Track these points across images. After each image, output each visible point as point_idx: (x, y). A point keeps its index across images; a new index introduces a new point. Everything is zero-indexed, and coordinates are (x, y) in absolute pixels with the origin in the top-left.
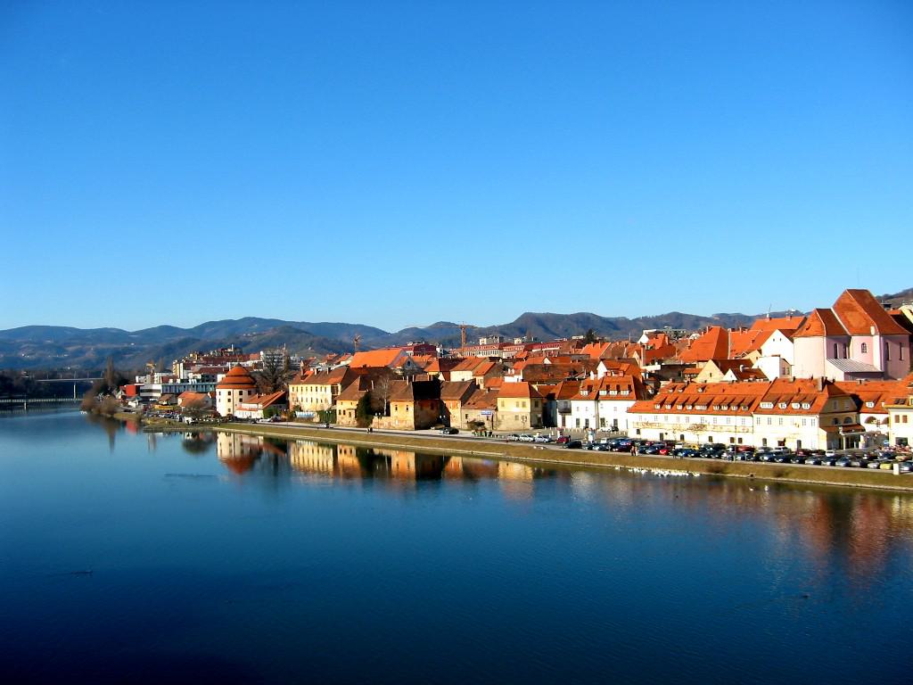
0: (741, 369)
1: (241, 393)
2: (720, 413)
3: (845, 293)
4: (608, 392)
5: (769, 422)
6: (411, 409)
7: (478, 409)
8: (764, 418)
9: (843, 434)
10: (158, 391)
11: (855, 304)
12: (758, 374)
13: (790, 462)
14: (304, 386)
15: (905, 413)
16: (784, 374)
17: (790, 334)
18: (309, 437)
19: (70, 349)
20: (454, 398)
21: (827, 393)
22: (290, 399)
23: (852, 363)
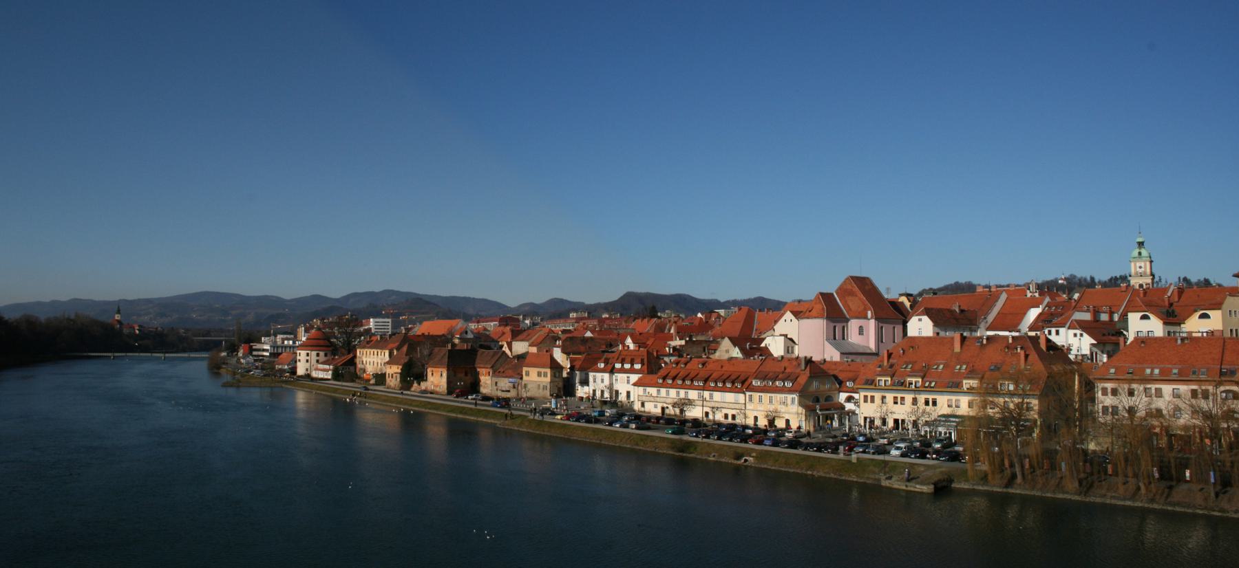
0: (748, 347)
1: (318, 355)
2: (716, 389)
3: (847, 279)
4: (623, 365)
5: (760, 399)
6: (445, 375)
7: (506, 377)
8: (756, 395)
9: (819, 413)
10: (267, 350)
11: (856, 289)
12: (766, 352)
13: (746, 442)
14: (368, 351)
15: (934, 397)
16: (788, 352)
17: (797, 314)
18: (375, 401)
19: (234, 312)
20: (486, 366)
21: (808, 372)
22: (358, 360)
23: (849, 344)
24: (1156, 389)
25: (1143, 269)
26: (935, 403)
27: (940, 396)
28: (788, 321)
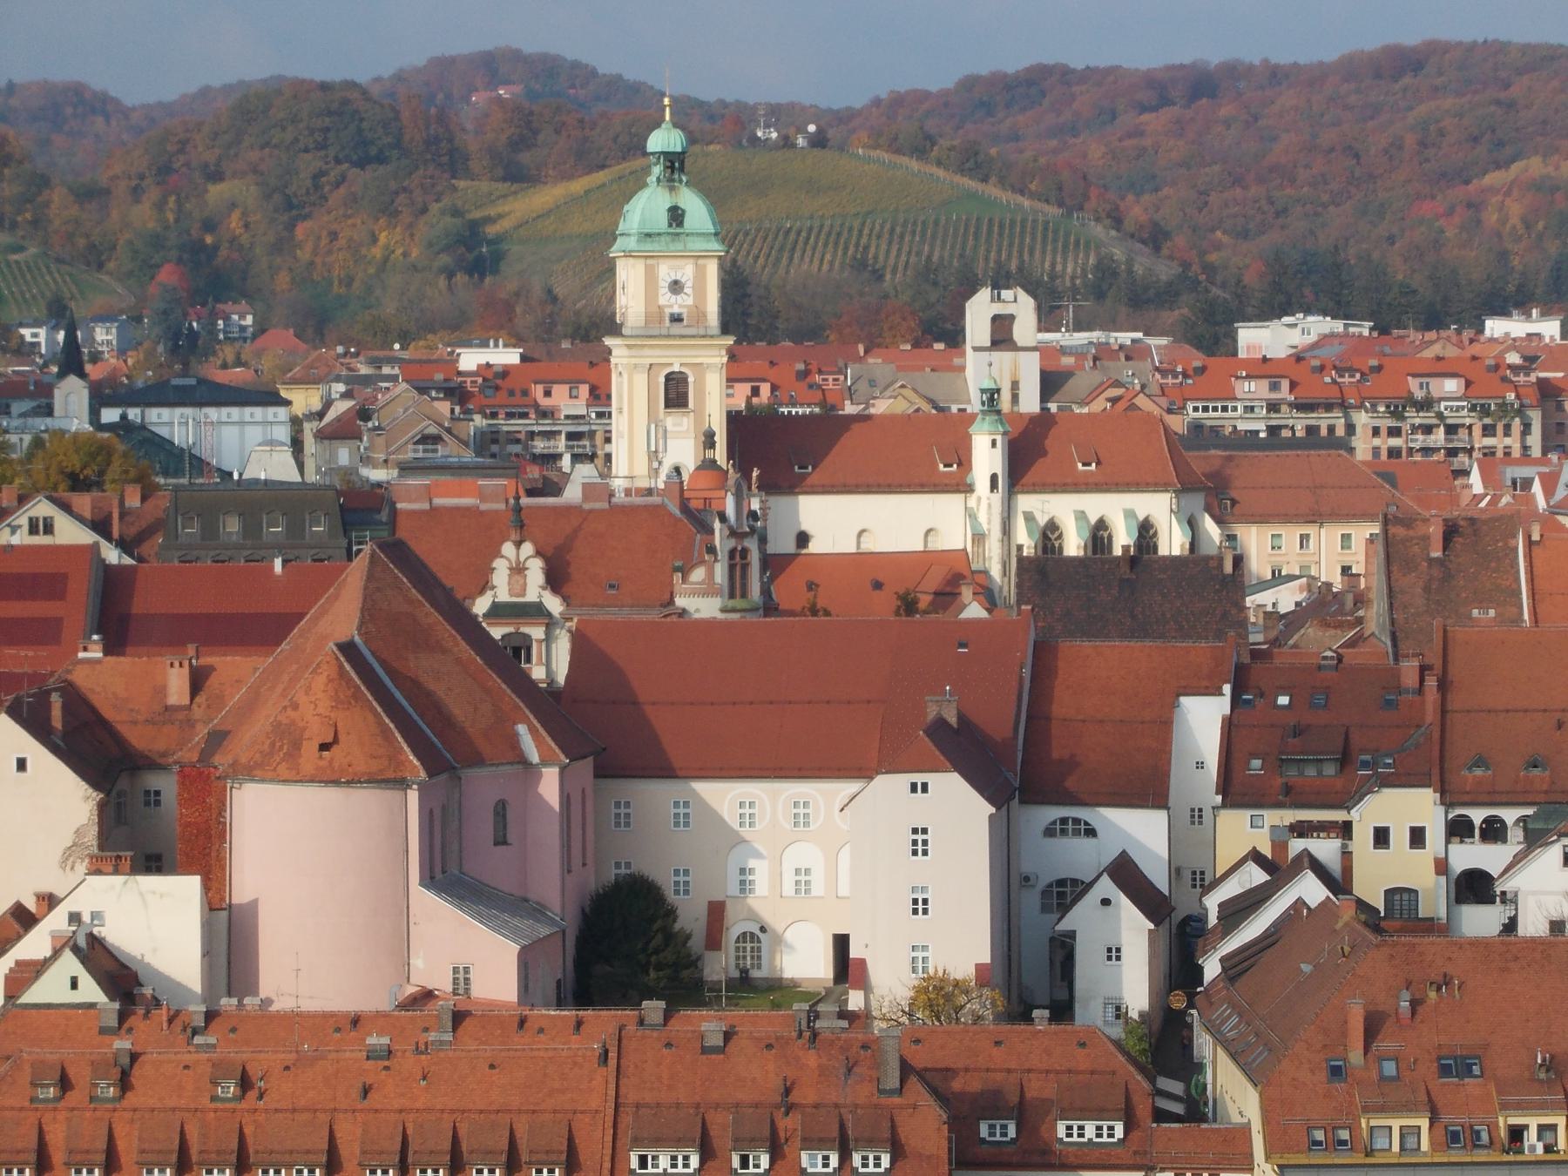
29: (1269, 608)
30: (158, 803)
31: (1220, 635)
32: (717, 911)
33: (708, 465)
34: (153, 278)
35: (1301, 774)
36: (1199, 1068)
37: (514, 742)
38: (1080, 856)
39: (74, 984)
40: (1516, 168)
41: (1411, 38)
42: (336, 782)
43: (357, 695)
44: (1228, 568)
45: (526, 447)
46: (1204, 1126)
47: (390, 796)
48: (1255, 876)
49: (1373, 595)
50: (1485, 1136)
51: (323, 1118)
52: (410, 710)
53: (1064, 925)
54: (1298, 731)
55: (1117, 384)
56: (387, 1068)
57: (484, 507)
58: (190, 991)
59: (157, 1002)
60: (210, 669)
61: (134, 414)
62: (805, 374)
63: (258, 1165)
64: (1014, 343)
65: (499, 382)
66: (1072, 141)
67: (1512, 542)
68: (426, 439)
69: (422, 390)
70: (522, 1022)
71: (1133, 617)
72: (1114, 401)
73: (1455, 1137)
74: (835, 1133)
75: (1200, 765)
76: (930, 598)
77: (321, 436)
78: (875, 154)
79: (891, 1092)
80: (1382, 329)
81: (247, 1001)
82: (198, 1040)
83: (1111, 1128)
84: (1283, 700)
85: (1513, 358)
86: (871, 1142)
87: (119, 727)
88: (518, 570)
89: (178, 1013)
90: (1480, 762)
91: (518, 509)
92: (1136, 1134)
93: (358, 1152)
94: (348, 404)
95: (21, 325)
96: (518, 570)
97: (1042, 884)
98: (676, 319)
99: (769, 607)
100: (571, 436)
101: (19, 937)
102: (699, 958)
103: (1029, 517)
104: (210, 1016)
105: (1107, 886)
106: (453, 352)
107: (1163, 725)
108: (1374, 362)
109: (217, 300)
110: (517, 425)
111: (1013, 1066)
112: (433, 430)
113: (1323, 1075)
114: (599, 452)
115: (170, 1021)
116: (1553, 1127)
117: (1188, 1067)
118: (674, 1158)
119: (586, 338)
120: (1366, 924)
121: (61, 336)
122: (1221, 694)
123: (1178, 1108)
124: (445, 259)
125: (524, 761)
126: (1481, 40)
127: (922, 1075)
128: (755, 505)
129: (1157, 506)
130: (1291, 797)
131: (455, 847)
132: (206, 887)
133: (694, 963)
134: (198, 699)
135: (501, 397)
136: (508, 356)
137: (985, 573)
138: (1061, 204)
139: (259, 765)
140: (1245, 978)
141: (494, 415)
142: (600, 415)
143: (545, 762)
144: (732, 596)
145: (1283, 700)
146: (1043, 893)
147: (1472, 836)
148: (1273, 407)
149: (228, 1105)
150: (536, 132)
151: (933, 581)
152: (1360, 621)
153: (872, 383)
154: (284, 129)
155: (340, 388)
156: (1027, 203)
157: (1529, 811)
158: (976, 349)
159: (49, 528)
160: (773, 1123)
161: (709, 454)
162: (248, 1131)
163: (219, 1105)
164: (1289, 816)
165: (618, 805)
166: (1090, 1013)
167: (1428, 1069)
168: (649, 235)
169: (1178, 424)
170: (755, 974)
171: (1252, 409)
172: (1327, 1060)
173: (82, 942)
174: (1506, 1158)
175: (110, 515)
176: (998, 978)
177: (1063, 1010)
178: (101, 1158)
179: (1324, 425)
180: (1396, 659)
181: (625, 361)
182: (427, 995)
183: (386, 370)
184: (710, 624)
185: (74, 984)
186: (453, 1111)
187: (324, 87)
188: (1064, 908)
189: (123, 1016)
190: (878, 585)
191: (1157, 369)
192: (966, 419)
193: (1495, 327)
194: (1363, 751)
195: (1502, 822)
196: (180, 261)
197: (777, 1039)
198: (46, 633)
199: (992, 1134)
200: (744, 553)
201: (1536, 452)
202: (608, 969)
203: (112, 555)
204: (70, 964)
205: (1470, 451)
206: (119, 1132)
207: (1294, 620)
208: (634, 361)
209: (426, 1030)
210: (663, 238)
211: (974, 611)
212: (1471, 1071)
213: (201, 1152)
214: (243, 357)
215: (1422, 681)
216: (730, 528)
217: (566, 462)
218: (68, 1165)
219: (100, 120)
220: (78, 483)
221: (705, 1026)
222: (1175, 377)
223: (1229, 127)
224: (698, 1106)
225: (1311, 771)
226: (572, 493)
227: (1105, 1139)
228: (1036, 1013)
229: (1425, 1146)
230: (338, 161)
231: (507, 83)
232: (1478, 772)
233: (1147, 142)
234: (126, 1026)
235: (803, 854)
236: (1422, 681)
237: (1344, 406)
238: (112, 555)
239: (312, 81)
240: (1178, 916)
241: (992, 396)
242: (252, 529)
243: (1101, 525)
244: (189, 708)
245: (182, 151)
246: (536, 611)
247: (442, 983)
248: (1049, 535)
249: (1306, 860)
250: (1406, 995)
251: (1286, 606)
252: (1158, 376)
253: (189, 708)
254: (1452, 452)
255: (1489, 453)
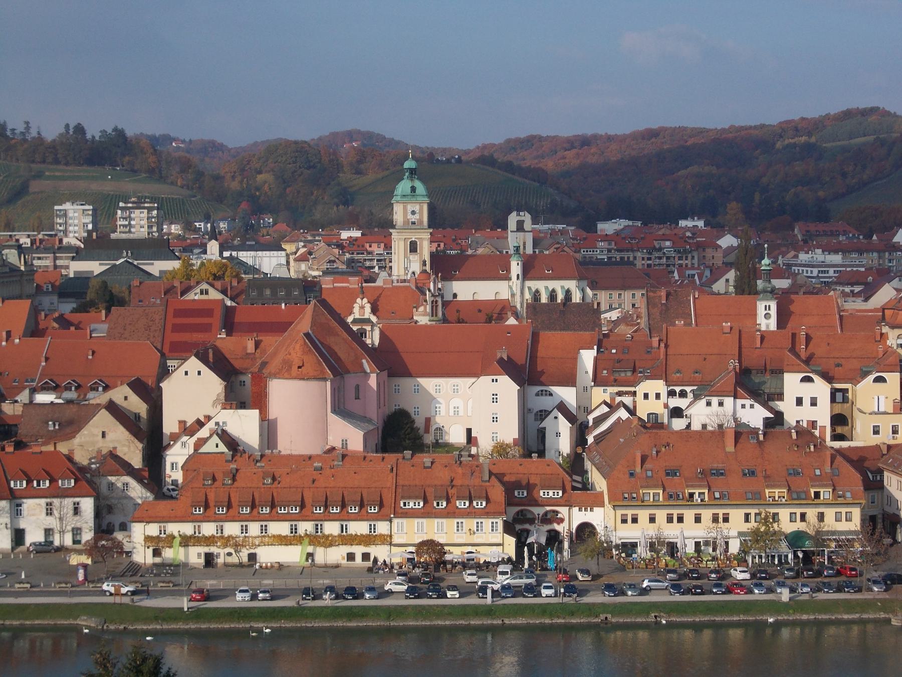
24: (815, 492)
25: (417, 216)
26: (726, 520)
27: (827, 509)
28: (193, 373)
29: (609, 319)
30: (244, 385)
31: (593, 329)
32: (428, 421)
33: (424, 271)
34: (239, 206)
35: (620, 375)
36: (586, 472)
37: (361, 365)
38: (546, 403)
39: (217, 446)
40: (689, 169)
41: (654, 125)
42: (303, 379)
43: (310, 350)
44: (595, 307)
45: (363, 264)
46: (588, 492)
47: (322, 383)
48: (606, 409)
49: (643, 315)
50: (681, 496)
51: (299, 490)
52: (327, 355)
53: (542, 425)
54: (619, 361)
55: (558, 243)
56: (320, 474)
57: (351, 287)
58: (254, 448)
59: (244, 452)
60: (261, 341)
61: (234, 254)
62: (454, 240)
63: (278, 506)
64: (524, 229)
65: (354, 242)
66: (542, 160)
67: (689, 298)
68: (330, 262)
69: (329, 245)
70: (365, 458)
71: (564, 323)
72: (557, 249)
73: (671, 496)
74: (468, 495)
75: (587, 372)
76: (496, 315)
77: (296, 260)
78: (478, 165)
79: (486, 481)
80: (645, 224)
81: (274, 451)
82: (258, 464)
83: (558, 493)
84: (614, 351)
85: (688, 234)
86: (480, 498)
87: (231, 361)
88: (362, 307)
89: (251, 455)
90: (679, 371)
91: (362, 287)
92: (566, 495)
93: (311, 501)
94: (305, 249)
95: (196, 222)
96: (362, 307)
97: (535, 411)
98: (413, 223)
99: (445, 320)
100: (378, 260)
101: (199, 430)
102: (422, 436)
103: (529, 288)
104: (262, 456)
105: (556, 412)
106: (339, 232)
107: (574, 360)
108: (642, 236)
109: (260, 214)
110: (360, 257)
111: (526, 472)
112: (333, 258)
113: (628, 476)
114: (388, 266)
115: (249, 458)
116: (704, 493)
117: (583, 472)
118: (415, 503)
119: (382, 227)
120: (641, 426)
121: (209, 225)
122: (594, 349)
123: (579, 486)
124: (336, 200)
125: (365, 372)
126: (678, 126)
127: (496, 475)
128: (440, 286)
129: (571, 285)
130: (616, 383)
131: (342, 400)
132: (261, 413)
133: (420, 438)
134: (257, 351)
135: (355, 247)
136: (357, 234)
137: (515, 307)
138: (539, 182)
139: (278, 373)
140: (601, 443)
141: (353, 254)
142: (387, 253)
143: (372, 372)
144: (432, 316)
145: (614, 351)
146: (535, 414)
147: (676, 396)
148: (609, 251)
149: (270, 486)
150: (365, 158)
151: (497, 310)
152: (638, 324)
153: (477, 243)
154: (282, 157)
155: (302, 244)
156: (527, 181)
157: (695, 388)
158: (511, 232)
159: (207, 293)
160: (447, 492)
161: (424, 268)
162: (275, 494)
163: (265, 486)
164: (616, 389)
165: (395, 386)
166: (550, 454)
167: (662, 474)
168: (404, 195)
169: (578, 256)
170: (440, 441)
171: (602, 251)
172: (629, 471)
173: (220, 432)
174: (688, 503)
175: (227, 288)
176: (520, 442)
177: (542, 453)
178: (226, 504)
179: (626, 256)
180: (651, 338)
181: (396, 237)
182: (333, 449)
183: (317, 238)
184: (425, 326)
185: (217, 446)
186: (342, 488)
187: (296, 143)
188: (542, 420)
189: (233, 456)
190: (480, 311)
191: (571, 238)
192: (508, 256)
193: (683, 223)
194: (639, 368)
195: (686, 391)
196: (248, 201)
197: (449, 464)
198: (206, 328)
199: (519, 495)
200: (436, 302)
201: (696, 266)
202: (393, 440)
203: (229, 303)
204: (216, 439)
205: (674, 265)
206: (232, 495)
207: (616, 323)
208: (400, 237)
209: (333, 460)
210: (409, 197)
211: (512, 321)
212: (676, 474)
213: (259, 502)
214: (270, 233)
215: (659, 345)
216: (432, 293)
217: (376, 269)
218: (215, 506)
219: (220, 152)
220: (216, 277)
221: (425, 460)
222: (577, 241)
223: (594, 156)
224: (423, 486)
225: (623, 374)
226: (379, 283)
227: (556, 496)
228: (533, 455)
229: (661, 499)
230: (300, 167)
231: (356, 141)
232: (678, 375)
233: (567, 161)
234: (234, 459)
235: (457, 402)
236: (659, 345)
237: (633, 251)
238: (229, 303)
239: (291, 141)
240: (579, 422)
241: (517, 249)
242: (274, 293)
243: (553, 291)
244: (254, 354)
245: (248, 164)
246: (368, 321)
247: (338, 444)
248: (536, 295)
249: (621, 404)
250: (655, 450)
251: (614, 318)
252: (571, 240)
253: (254, 354)
254: (668, 266)
255: (681, 266)
